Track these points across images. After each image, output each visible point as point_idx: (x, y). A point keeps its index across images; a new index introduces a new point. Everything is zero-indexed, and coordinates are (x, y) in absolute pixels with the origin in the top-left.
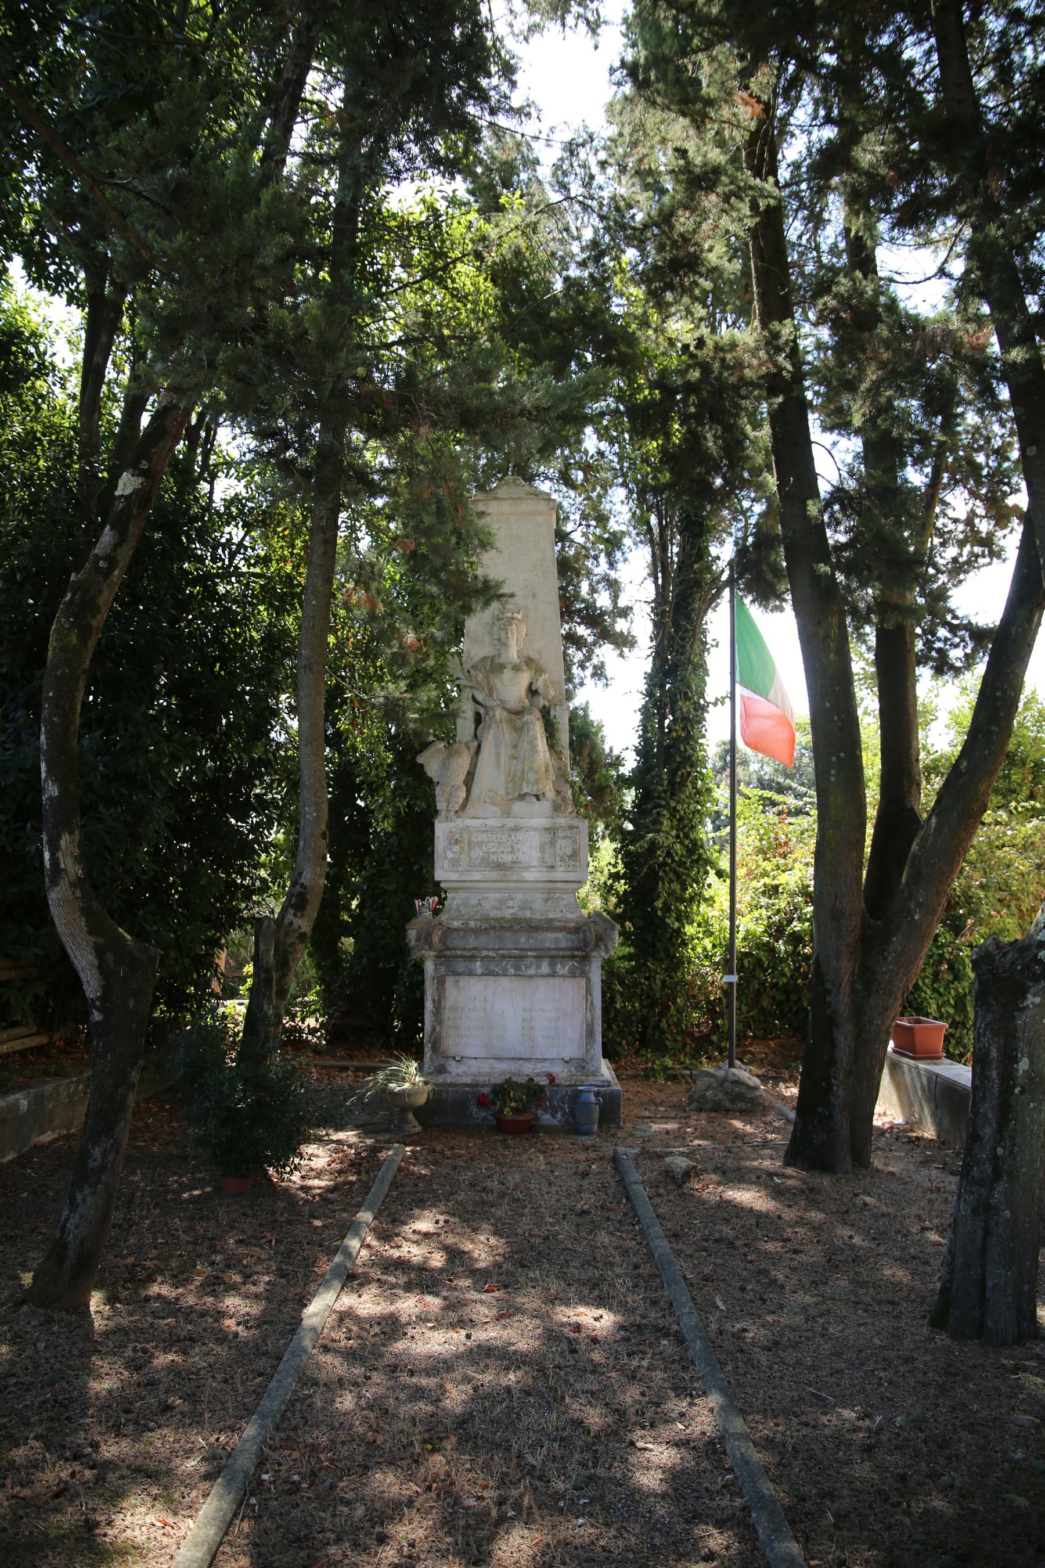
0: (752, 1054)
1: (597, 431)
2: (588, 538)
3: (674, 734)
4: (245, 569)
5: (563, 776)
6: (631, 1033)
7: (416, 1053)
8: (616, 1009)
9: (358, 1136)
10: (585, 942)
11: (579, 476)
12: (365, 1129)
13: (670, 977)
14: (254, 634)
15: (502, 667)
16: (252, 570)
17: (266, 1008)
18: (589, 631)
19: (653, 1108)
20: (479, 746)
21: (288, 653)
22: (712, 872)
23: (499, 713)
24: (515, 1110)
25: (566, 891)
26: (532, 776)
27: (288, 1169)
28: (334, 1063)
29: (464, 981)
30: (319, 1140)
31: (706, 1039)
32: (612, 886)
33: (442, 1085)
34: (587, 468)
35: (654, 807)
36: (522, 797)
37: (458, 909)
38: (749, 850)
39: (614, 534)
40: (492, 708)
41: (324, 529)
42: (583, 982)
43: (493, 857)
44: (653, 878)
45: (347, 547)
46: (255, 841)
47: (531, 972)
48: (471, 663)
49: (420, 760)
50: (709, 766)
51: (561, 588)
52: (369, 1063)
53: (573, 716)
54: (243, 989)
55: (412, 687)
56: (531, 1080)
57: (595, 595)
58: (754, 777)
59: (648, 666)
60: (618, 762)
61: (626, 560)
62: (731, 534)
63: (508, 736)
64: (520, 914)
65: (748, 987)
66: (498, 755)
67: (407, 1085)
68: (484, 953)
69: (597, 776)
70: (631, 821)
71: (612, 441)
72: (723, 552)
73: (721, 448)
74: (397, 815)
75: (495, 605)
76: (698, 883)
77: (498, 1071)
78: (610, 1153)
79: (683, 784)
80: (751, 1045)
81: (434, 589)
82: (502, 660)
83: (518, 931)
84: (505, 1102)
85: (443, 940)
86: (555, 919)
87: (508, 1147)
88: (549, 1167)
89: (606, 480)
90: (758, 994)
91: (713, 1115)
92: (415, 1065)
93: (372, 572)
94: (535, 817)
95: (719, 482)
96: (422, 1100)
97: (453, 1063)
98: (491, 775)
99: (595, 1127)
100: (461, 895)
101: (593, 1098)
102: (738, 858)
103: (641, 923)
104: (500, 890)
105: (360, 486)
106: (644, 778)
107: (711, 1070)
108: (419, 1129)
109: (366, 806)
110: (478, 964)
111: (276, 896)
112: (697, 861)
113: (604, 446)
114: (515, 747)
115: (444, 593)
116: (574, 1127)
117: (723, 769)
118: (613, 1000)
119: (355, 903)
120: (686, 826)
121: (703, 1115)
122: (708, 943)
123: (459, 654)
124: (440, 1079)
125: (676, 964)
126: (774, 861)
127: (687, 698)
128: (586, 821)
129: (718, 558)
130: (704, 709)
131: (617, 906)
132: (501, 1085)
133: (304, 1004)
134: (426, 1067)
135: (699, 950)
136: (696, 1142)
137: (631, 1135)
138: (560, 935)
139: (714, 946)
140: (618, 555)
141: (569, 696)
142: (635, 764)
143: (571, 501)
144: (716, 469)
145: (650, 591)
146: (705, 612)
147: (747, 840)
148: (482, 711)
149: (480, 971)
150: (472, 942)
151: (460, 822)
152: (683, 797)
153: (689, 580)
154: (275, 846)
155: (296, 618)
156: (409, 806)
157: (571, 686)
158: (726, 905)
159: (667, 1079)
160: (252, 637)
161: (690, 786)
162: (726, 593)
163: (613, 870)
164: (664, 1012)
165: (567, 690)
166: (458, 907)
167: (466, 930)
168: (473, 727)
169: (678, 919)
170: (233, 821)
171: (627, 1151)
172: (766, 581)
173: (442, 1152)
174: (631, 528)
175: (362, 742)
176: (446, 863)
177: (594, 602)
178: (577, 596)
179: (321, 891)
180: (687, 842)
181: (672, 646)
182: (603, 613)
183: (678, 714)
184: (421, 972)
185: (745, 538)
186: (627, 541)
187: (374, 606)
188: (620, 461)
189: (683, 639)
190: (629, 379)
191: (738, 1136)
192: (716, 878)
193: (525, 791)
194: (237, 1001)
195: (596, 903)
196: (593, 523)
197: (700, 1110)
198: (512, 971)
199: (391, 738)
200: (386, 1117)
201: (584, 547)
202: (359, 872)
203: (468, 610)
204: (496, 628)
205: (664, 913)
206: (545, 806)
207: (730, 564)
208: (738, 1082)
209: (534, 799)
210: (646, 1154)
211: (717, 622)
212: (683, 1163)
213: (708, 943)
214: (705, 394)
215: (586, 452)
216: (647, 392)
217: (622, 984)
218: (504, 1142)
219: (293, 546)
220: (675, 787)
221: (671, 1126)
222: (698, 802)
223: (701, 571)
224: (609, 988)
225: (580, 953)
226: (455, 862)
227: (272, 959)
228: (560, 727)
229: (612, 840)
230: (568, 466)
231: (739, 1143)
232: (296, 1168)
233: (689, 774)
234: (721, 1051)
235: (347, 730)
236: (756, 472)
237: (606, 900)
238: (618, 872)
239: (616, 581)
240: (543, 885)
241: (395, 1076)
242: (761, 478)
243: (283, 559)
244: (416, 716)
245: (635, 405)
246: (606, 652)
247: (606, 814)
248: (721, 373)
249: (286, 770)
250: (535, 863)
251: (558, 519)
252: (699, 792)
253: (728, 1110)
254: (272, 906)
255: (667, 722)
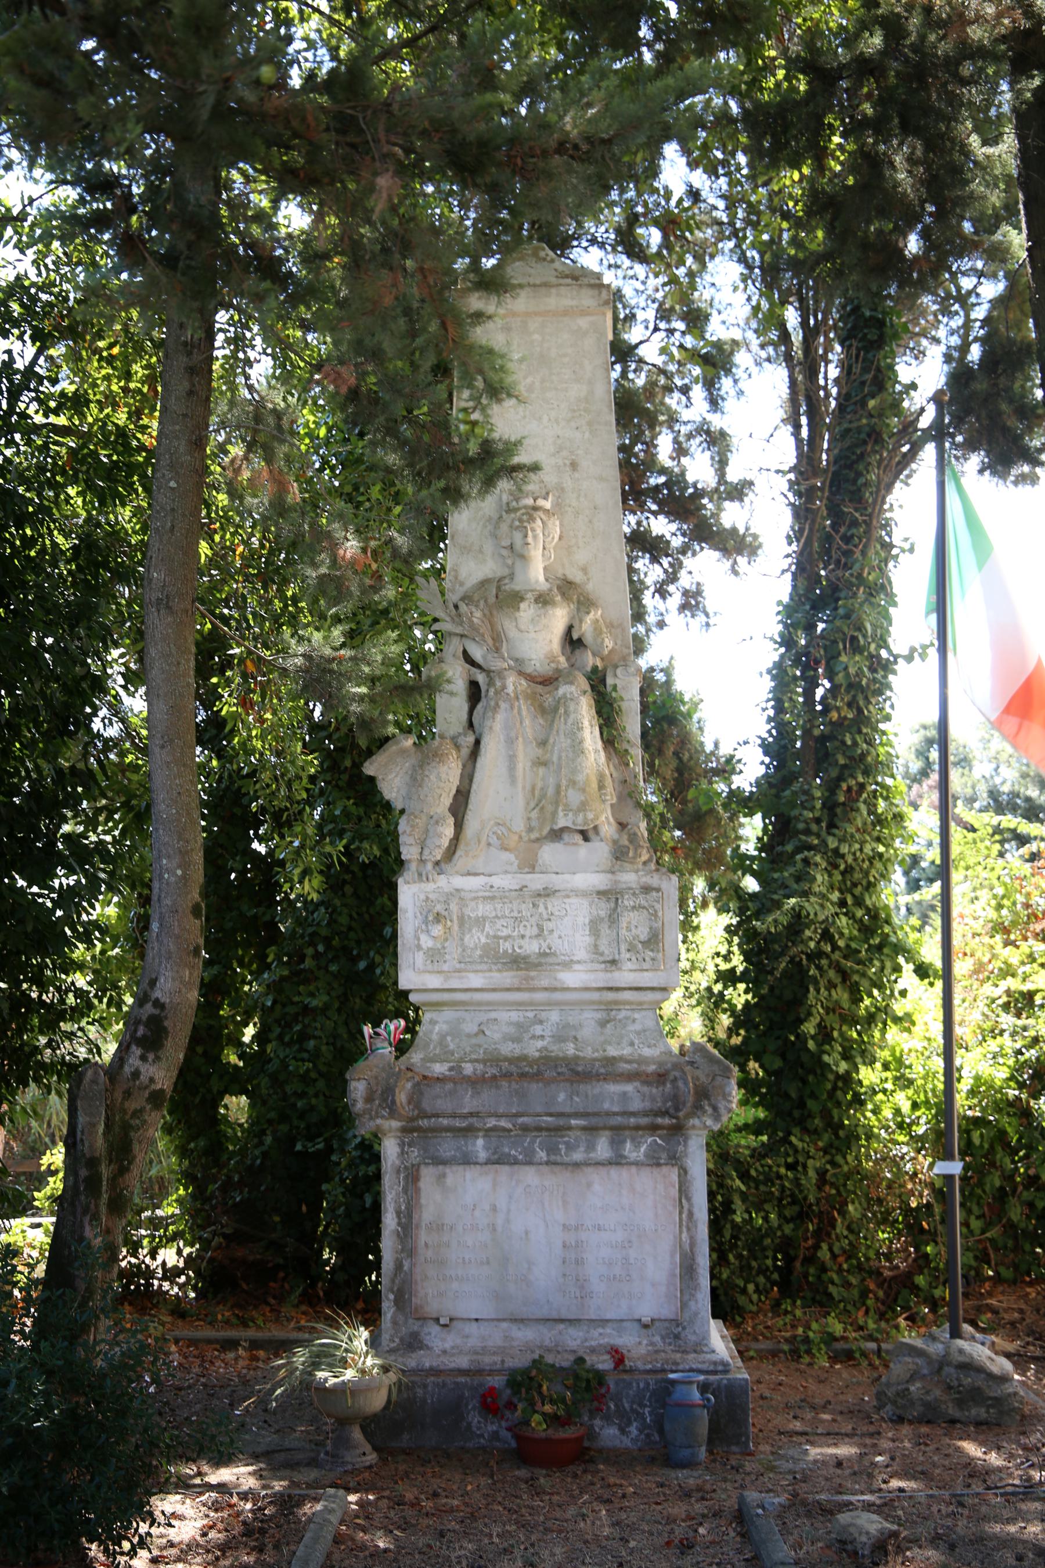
0: (995, 1312)
1: (686, 151)
2: (671, 356)
3: (834, 715)
4: (39, 419)
5: (630, 795)
6: (763, 1271)
7: (364, 1311)
8: (735, 1226)
9: (258, 1475)
10: (676, 1100)
11: (654, 237)
12: (271, 1460)
13: (833, 1163)
14: (60, 540)
15: (517, 598)
16: (53, 419)
17: (88, 1232)
18: (673, 527)
19: (809, 1415)
20: (477, 742)
21: (124, 575)
22: (908, 968)
23: (512, 683)
24: (553, 1420)
25: (640, 1006)
26: (574, 797)
27: (126, 1545)
28: (209, 1333)
29: (454, 1175)
30: (183, 1486)
31: (905, 1281)
32: (721, 994)
33: (414, 1372)
34: (669, 224)
35: (798, 850)
36: (557, 835)
37: (442, 1042)
38: (978, 926)
39: (718, 345)
40: (500, 673)
41: (188, 348)
42: (674, 1174)
43: (505, 946)
44: (798, 979)
45: (229, 373)
46: (67, 920)
47: (578, 1156)
48: (460, 591)
49: (370, 769)
50: (899, 770)
51: (622, 448)
52: (277, 1333)
53: (648, 683)
54: (40, 1198)
55: (353, 637)
56: (580, 1360)
57: (684, 461)
58: (982, 790)
59: (783, 589)
60: (728, 768)
61: (740, 393)
62: (937, 341)
63: (529, 724)
64: (556, 1050)
65: (981, 1184)
66: (512, 759)
67: (349, 1374)
68: (491, 1122)
69: (691, 794)
70: (754, 874)
71: (712, 172)
72: (922, 374)
73: (922, 182)
74: (327, 871)
75: (504, 485)
76: (881, 987)
77: (519, 1345)
78: (732, 1503)
79: (850, 806)
80: (990, 1294)
81: (393, 459)
82: (517, 586)
83: (553, 1080)
84: (532, 1404)
85: (415, 1099)
86: (621, 1059)
87: (539, 1493)
88: (617, 1532)
89: (704, 244)
90: (1001, 1196)
91: (924, 1429)
92: (364, 1334)
93: (279, 427)
94: (580, 871)
95: (913, 244)
96: (377, 1401)
97: (435, 1329)
98: (501, 792)
99: (702, 1453)
100: (448, 1014)
101: (696, 1396)
102: (957, 941)
103: (778, 1064)
104: (519, 1005)
105: (266, 285)
106: (777, 796)
107: (919, 1343)
108: (372, 1458)
109: (271, 853)
110: (480, 1142)
111: (103, 1023)
112: (879, 948)
113: (699, 179)
114: (543, 743)
115: (411, 465)
116: (662, 1453)
117: (924, 773)
118: (727, 1208)
119: (249, 1032)
120: (857, 884)
121: (906, 1430)
122: (902, 1100)
123: (438, 573)
124: (412, 1361)
125: (844, 1139)
126: (1025, 947)
127: (856, 648)
128: (675, 878)
129: (913, 386)
130: (887, 667)
131: (731, 1031)
132: (525, 1372)
133: (155, 1223)
134: (385, 1337)
135: (887, 1113)
136: (895, 1483)
137: (772, 1469)
138: (629, 1088)
139: (915, 1106)
140: (726, 384)
141: (639, 646)
142: (762, 770)
143: (639, 285)
144: (910, 219)
145: (785, 451)
146: (889, 488)
147: (972, 910)
148: (481, 678)
149: (483, 1155)
150: (469, 1102)
151: (444, 883)
152: (851, 829)
153: (859, 430)
154: (104, 931)
155: (137, 511)
156: (347, 852)
157: (641, 629)
158: (937, 1030)
159: (834, 1359)
160: (55, 545)
161: (863, 808)
162: (929, 452)
163: (724, 966)
164: (824, 1232)
165: (635, 636)
166: (443, 1037)
167: (456, 1079)
168: (466, 708)
169: (846, 1056)
170: (21, 883)
171: (765, 1499)
172: (1005, 430)
173: (415, 1504)
174: (751, 335)
175: (262, 737)
176: (420, 958)
177: (683, 474)
178: (650, 463)
179: (191, 1012)
180: (859, 913)
181: (828, 552)
182: (699, 494)
183: (840, 678)
184: (376, 1158)
185: (964, 348)
186: (742, 358)
187: (282, 488)
188: (731, 207)
189: (847, 539)
190: (748, 51)
191: (975, 1472)
192: (915, 979)
193: (562, 823)
194: (26, 1221)
195: (692, 1026)
196: (680, 325)
197: (899, 1420)
198: (542, 1155)
199: (315, 728)
200: (309, 1437)
201: (662, 371)
202: (257, 975)
203: (455, 495)
204: (504, 527)
205: (819, 1045)
206: (599, 851)
207: (937, 398)
208: (969, 1367)
209: (578, 838)
210: (801, 1506)
211: (910, 505)
212: (872, 1524)
213: (902, 1100)
214: (892, 80)
215: (668, 194)
216: (781, 74)
217: (744, 1176)
218: (531, 1481)
219: (128, 376)
220: (835, 813)
221: (845, 1450)
222: (878, 840)
223: (881, 414)
224: (721, 1185)
225: (667, 1121)
226: (435, 955)
227: (100, 1142)
228: (624, 705)
229: (722, 910)
230: (633, 220)
231: (978, 1488)
232: (142, 1544)
233: (862, 787)
234: (934, 1306)
235: (235, 716)
236: (988, 224)
237: (710, 1021)
238: (733, 970)
239: (723, 434)
240: (595, 996)
241: (324, 1358)
242: (998, 237)
243: (110, 400)
244: (363, 690)
245: (758, 105)
246: (704, 565)
247: (708, 862)
248: (923, 38)
249: (123, 790)
250: (581, 954)
251: (616, 319)
252: (880, 821)
253: (953, 1422)
254: (99, 1041)
255: (819, 692)
